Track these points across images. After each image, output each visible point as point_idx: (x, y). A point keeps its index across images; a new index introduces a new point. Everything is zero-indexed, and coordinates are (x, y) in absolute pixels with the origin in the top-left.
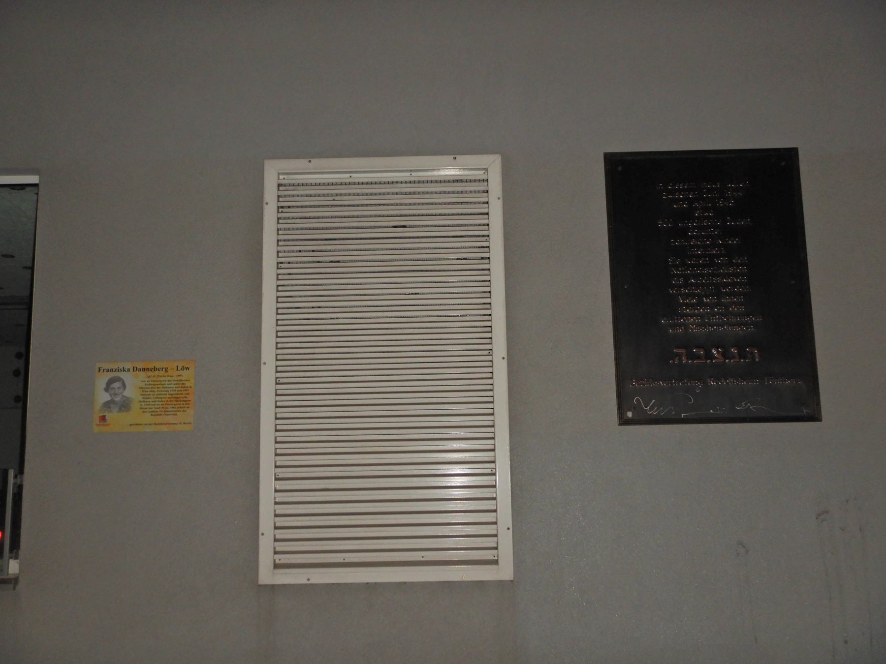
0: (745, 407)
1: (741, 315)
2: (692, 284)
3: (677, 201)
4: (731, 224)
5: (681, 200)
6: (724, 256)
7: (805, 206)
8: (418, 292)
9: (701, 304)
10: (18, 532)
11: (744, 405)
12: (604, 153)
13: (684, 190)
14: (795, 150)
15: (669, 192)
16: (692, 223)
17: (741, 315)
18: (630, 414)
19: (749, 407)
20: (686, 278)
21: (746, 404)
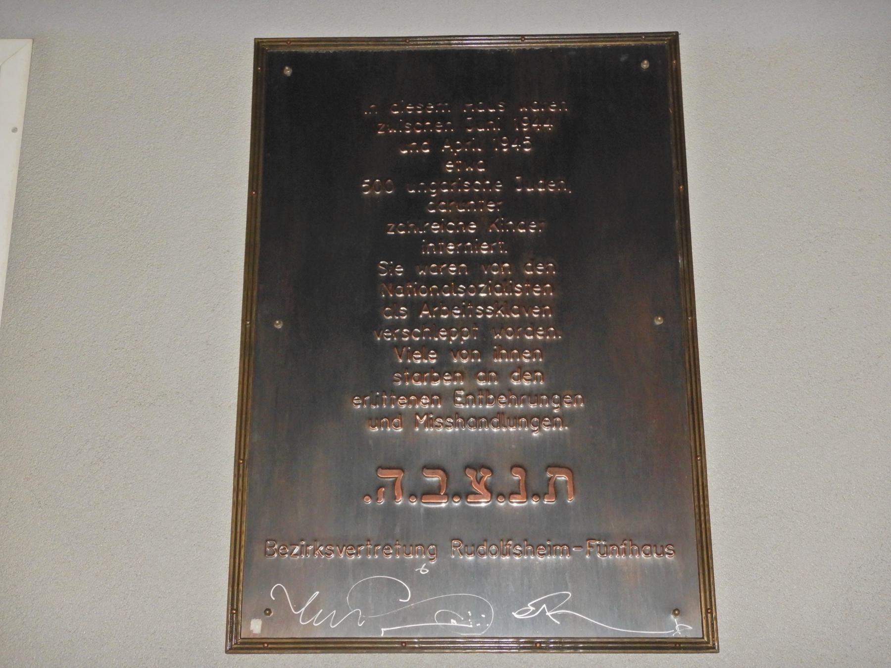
0: (534, 612)
1: (533, 395)
2: (426, 322)
4: (524, 192)
6: (501, 260)
7: (248, 143)
11: (532, 609)
12: (255, 39)
13: (424, 118)
14: (673, 39)
15: (394, 122)
16: (439, 187)
17: (533, 395)
18: (256, 627)
19: (544, 611)
20: (415, 306)
21: (537, 606)
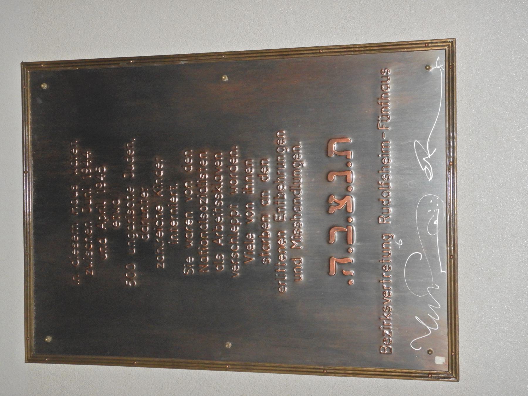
0: (428, 166)
1: (277, 166)
2: (227, 241)
3: (99, 256)
4: (134, 172)
5: (96, 249)
8: (459, 163)
9: (259, 229)
10: (432, 181)
11: (426, 167)
15: (85, 263)
18: (441, 361)
20: (215, 249)
